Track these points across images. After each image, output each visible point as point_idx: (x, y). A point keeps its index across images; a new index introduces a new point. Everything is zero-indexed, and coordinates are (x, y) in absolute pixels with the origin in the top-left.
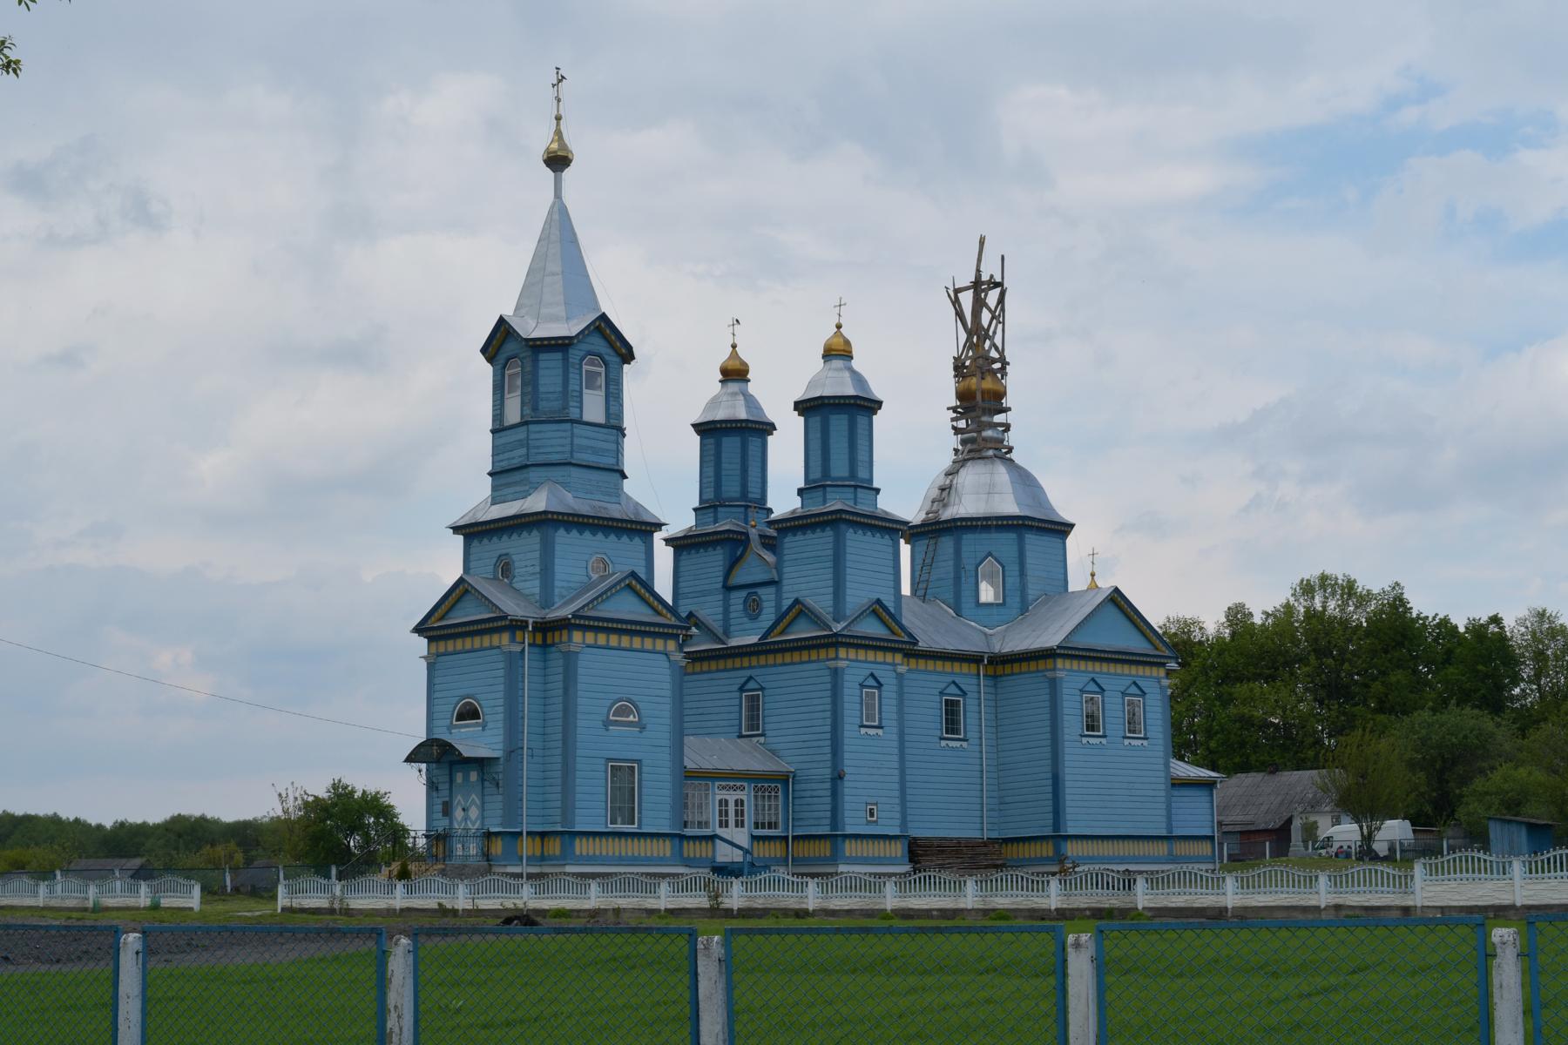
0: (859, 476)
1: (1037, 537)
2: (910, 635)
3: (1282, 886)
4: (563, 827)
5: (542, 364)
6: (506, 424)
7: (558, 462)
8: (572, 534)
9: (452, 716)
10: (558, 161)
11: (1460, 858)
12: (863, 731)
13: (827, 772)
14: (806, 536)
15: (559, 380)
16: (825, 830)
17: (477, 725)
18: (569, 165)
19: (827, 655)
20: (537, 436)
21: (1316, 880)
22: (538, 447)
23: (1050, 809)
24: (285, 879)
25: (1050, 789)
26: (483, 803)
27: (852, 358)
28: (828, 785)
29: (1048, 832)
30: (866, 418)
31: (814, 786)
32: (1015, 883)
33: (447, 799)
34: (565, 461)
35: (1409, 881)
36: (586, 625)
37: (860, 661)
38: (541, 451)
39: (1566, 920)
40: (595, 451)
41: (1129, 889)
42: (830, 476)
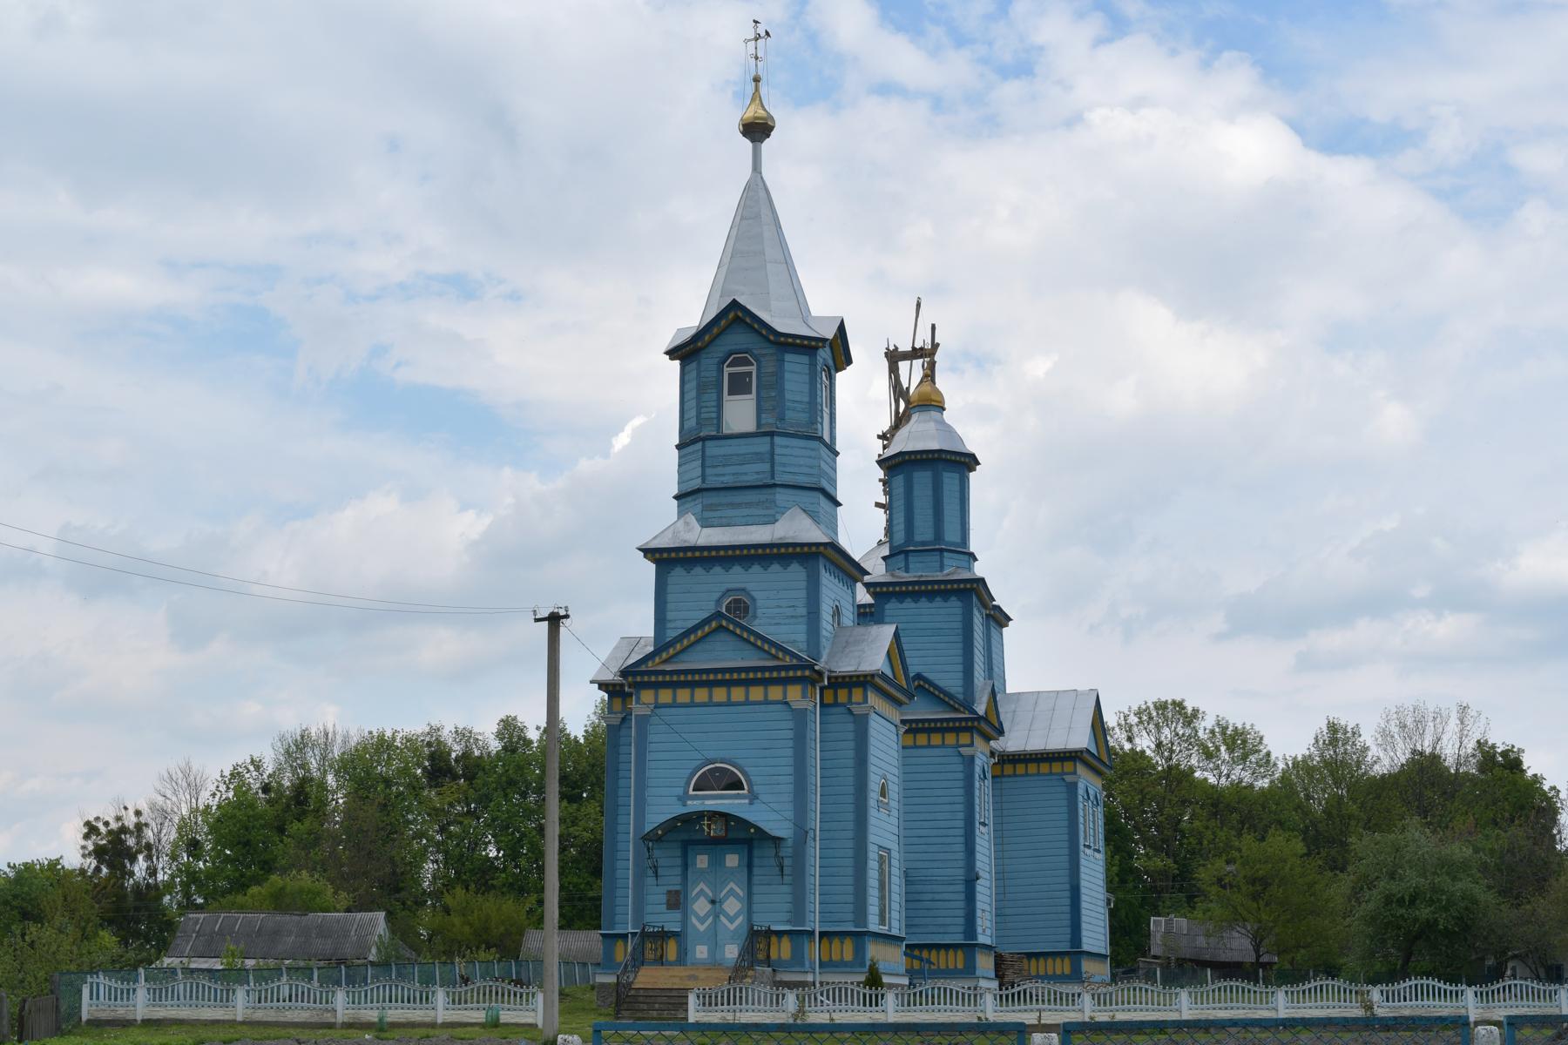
0: (946, 539)
2: (1001, 724)
3: (939, 1004)
4: (856, 927)
5: (787, 366)
6: (726, 431)
7: (809, 485)
8: (789, 569)
9: (690, 779)
10: (757, 130)
11: (1225, 987)
13: (960, 873)
14: (919, 605)
15: (806, 388)
16: (958, 939)
17: (742, 797)
18: (768, 136)
19: (958, 741)
20: (784, 451)
21: (533, 997)
22: (784, 465)
23: (1068, 923)
24: (146, 980)
25: (1067, 901)
26: (750, 894)
27: (944, 409)
28: (961, 888)
29: (1064, 947)
30: (957, 476)
31: (940, 889)
32: (481, 995)
33: (678, 888)
34: (813, 486)
35: (231, 994)
36: (766, 679)
38: (788, 469)
39: (1193, 1044)
41: (778, 1003)
42: (944, 540)
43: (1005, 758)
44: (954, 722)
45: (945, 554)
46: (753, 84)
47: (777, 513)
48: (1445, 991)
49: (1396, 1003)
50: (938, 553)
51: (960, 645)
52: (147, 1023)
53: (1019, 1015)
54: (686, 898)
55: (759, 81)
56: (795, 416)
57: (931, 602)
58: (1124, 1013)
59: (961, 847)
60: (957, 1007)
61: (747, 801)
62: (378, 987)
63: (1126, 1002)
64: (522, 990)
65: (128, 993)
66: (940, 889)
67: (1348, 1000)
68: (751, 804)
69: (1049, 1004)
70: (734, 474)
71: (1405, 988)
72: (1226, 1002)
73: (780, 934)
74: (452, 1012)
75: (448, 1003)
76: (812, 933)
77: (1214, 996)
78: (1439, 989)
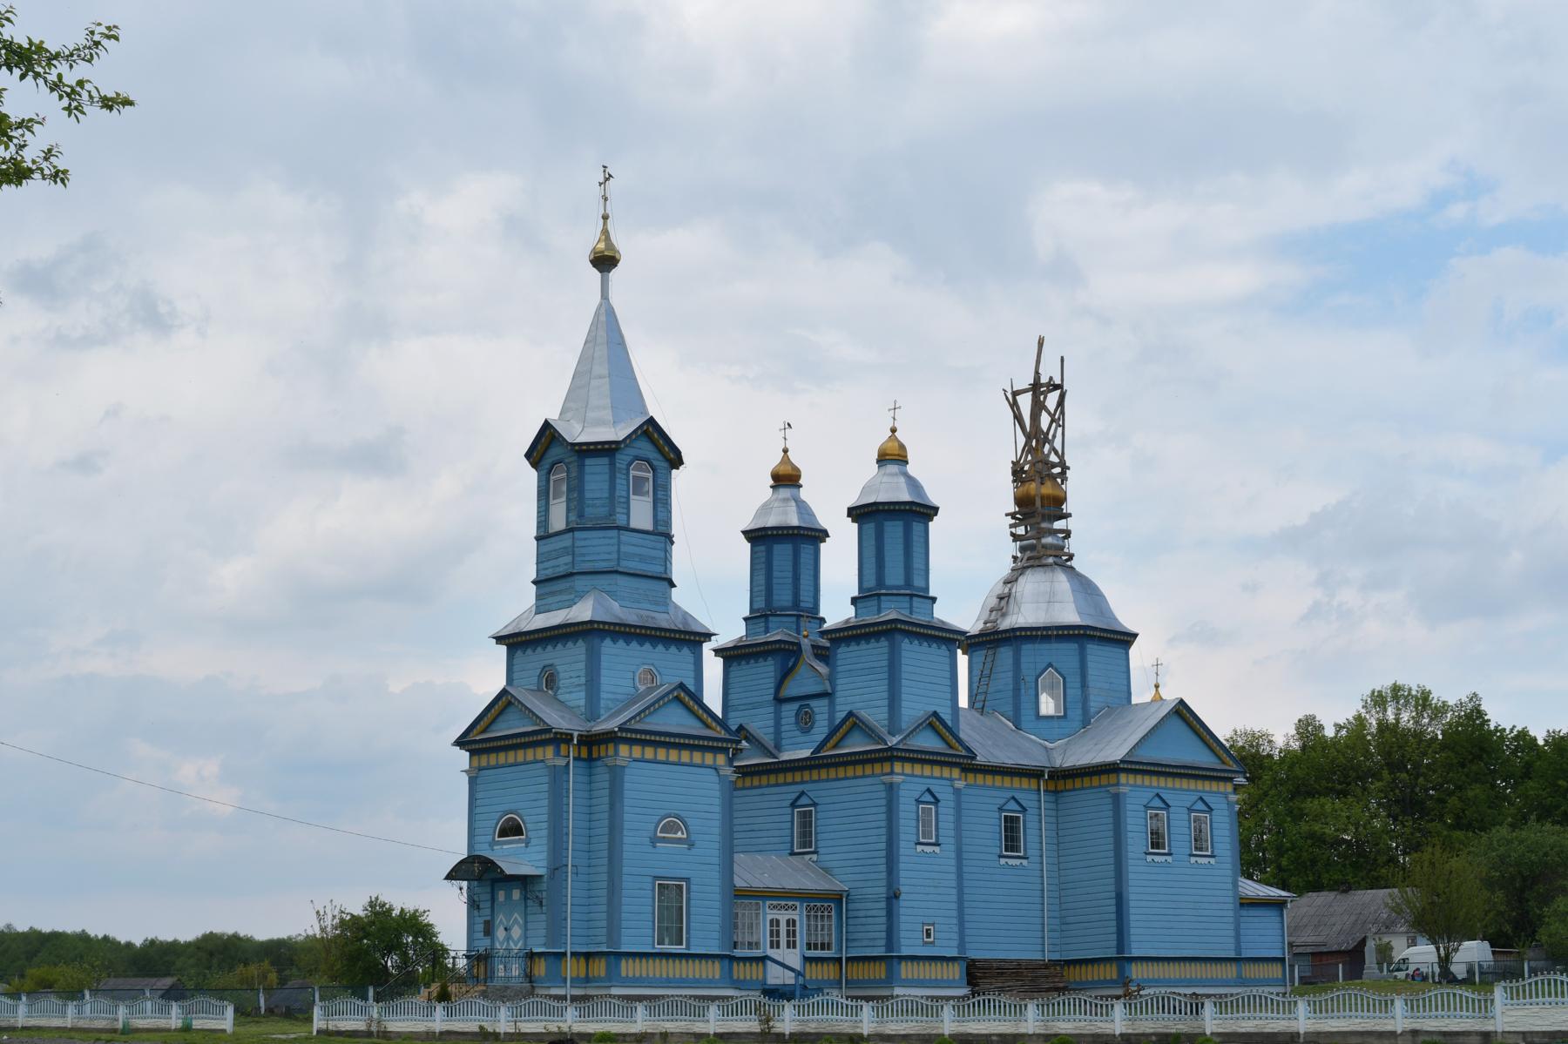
1: (1100, 647)
2: (968, 749)
6: (551, 531)
10: (605, 262)
12: (920, 848)
13: (882, 891)
15: (606, 486)
16: (880, 951)
21: (1392, 1004)
22: (583, 555)
26: (526, 922)
27: (907, 462)
28: (883, 905)
31: (869, 905)
33: (488, 918)
34: (612, 569)
37: (916, 776)
40: (642, 559)
43: (1059, 774)
44: (867, 755)
45: (882, 598)
46: (602, 220)
47: (576, 597)
48: (847, 1006)
49: (806, 1017)
50: (907, 598)
51: (886, 682)
52: (24, 1028)
53: (604, 1025)
54: (493, 926)
55: (607, 219)
56: (595, 511)
57: (868, 644)
58: (979, 1024)
59: (883, 868)
60: (1368, 1014)
61: (524, 845)
62: (463, 1003)
63: (1330, 1011)
64: (1107, 1003)
65: (1386, 1004)
66: (869, 905)
67: (1099, 1014)
68: (527, 847)
69: (1272, 1013)
70: (553, 567)
71: (525, 1005)
72: (1272, 1013)
73: (541, 954)
74: (1411, 1020)
75: (1407, 1011)
76: (565, 954)
77: (1327, 1005)
78: (927, 1006)
